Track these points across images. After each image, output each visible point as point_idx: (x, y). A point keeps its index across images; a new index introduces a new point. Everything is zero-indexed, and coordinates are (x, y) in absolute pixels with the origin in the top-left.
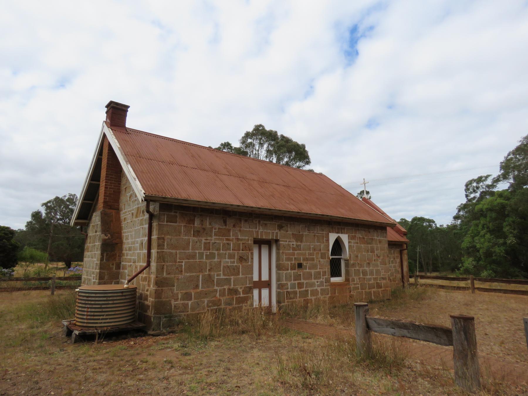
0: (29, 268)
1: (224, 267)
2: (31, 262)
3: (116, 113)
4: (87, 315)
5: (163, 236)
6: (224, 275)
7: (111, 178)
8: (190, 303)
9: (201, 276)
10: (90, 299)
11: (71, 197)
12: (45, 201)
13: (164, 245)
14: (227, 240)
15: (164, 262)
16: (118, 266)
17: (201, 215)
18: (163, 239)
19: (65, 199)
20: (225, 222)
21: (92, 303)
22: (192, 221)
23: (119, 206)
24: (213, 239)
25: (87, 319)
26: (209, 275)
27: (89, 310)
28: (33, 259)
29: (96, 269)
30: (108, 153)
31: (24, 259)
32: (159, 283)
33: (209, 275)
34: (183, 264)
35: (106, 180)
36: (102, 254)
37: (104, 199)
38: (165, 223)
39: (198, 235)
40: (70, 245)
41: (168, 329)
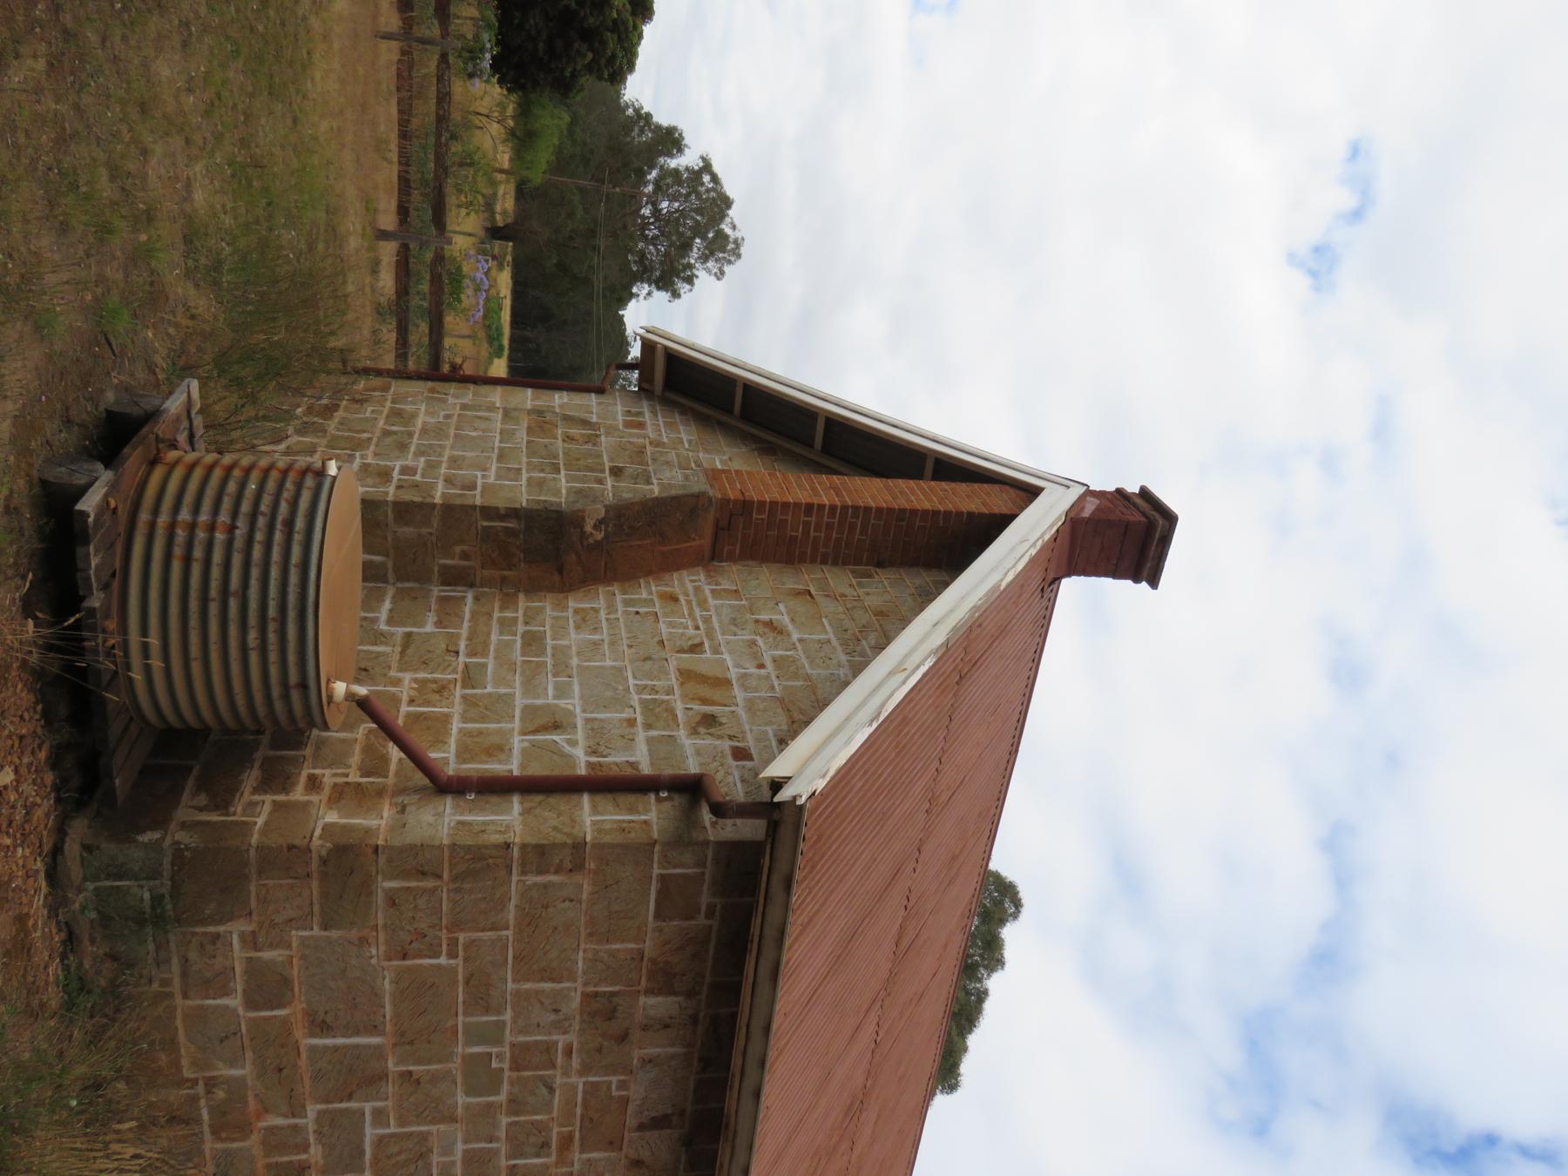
0: (495, 128)
1: (424, 1137)
2: (512, 133)
3: (1125, 537)
4: (192, 527)
5: (591, 865)
6: (380, 1142)
7: (852, 527)
8: (235, 1002)
9: (375, 1040)
10: (278, 536)
11: (731, 246)
12: (716, 168)
13: (540, 872)
14: (566, 1142)
15: (455, 879)
16: (454, 578)
17: (694, 1020)
18: (578, 866)
19: (723, 226)
20: (659, 1123)
21: (257, 552)
22: (663, 980)
23: (731, 558)
24: (571, 1081)
25: (172, 526)
26: (383, 1076)
27: (220, 536)
28: (523, 138)
29: (449, 481)
30: (959, 514)
31: (524, 111)
32: (347, 864)
33: (383, 1076)
34: (443, 960)
35: (845, 508)
36: (514, 513)
37: (762, 503)
38: (656, 871)
39: (593, 1015)
40: (571, 238)
41: (93, 915)
